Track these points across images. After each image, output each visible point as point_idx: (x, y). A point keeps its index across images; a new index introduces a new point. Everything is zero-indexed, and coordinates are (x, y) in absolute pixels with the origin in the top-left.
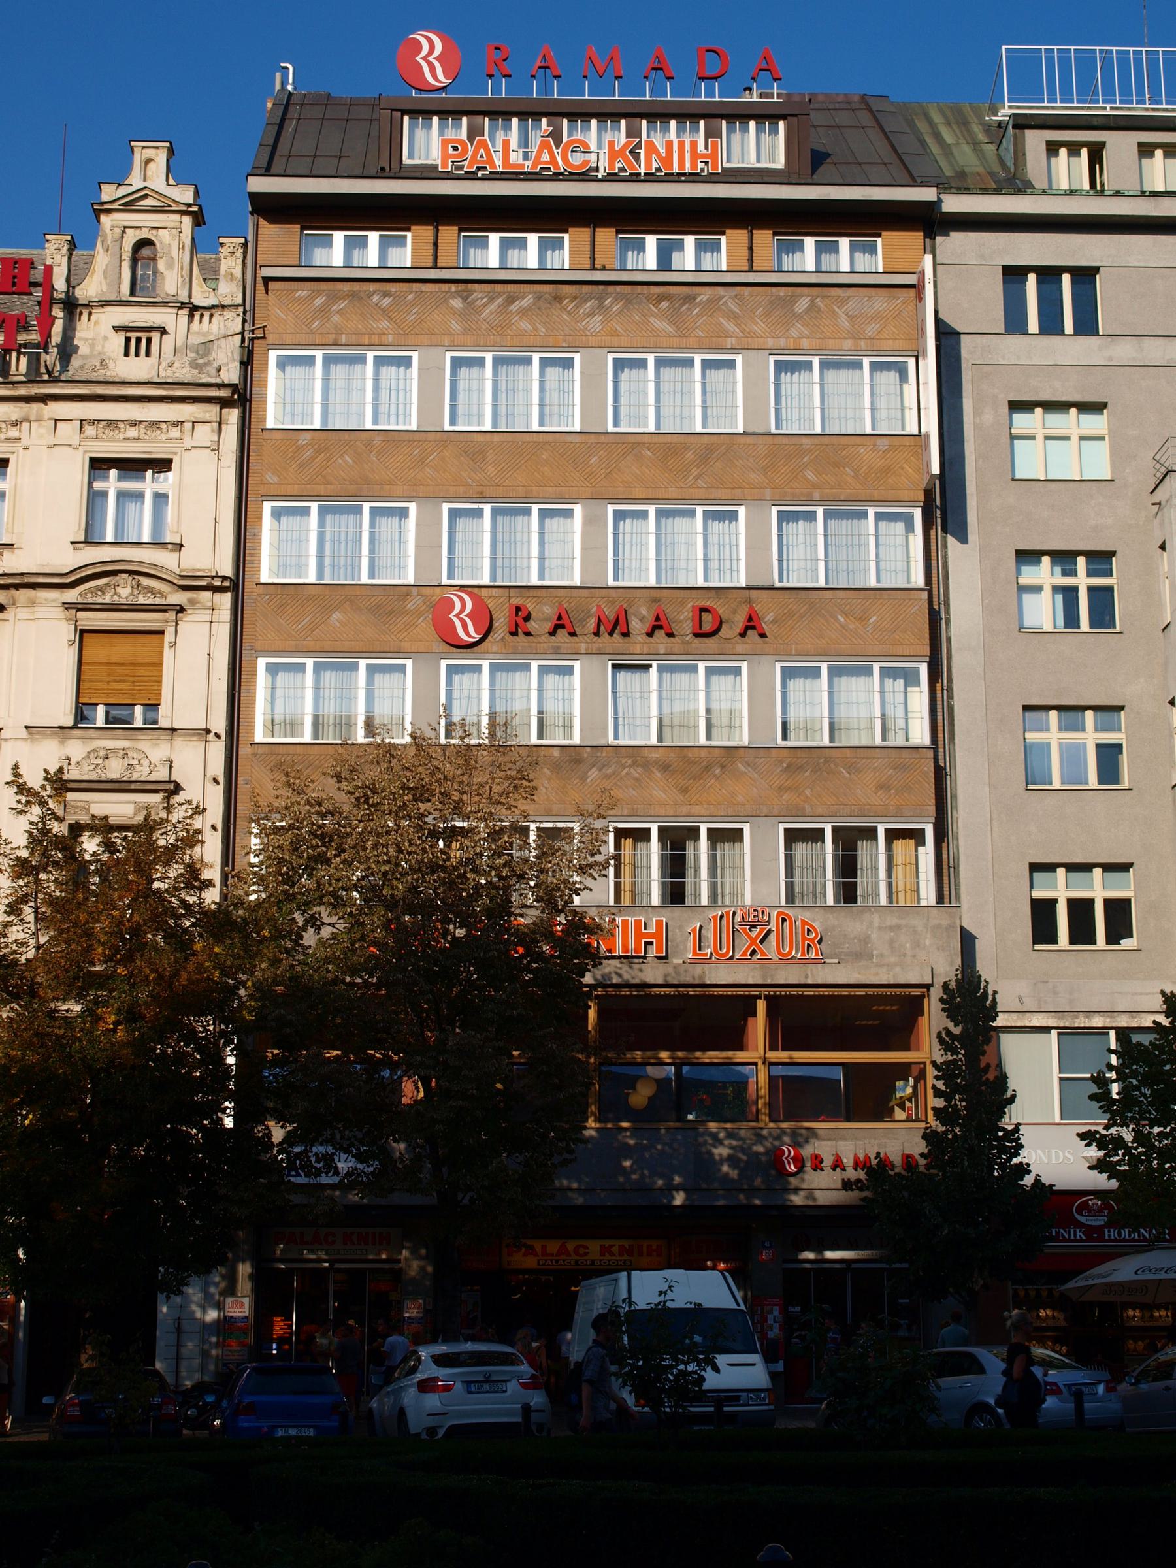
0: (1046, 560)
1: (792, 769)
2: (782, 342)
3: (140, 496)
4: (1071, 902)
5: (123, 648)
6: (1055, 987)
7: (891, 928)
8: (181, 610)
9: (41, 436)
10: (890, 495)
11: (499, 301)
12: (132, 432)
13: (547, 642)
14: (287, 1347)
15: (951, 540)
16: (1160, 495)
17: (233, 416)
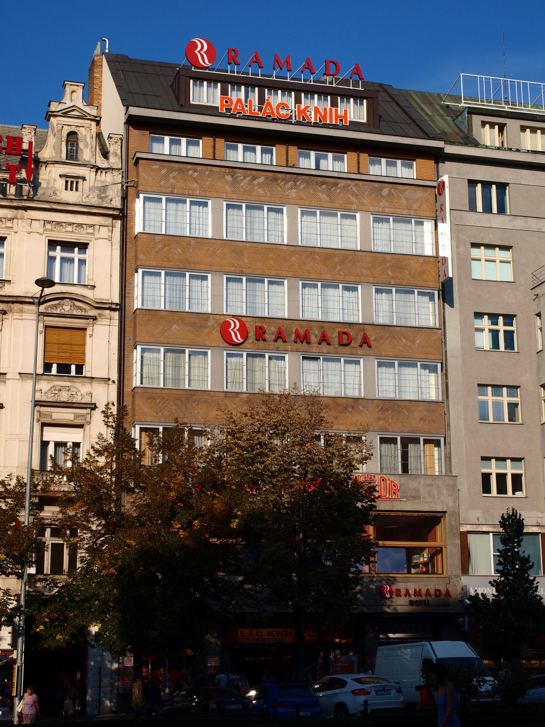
0: (486, 317)
1: (383, 410)
2: (377, 209)
3: (72, 260)
4: (513, 475)
5: (65, 336)
6: (492, 513)
7: (429, 485)
8: (95, 318)
9: (23, 227)
10: (424, 284)
11: (249, 178)
12: (69, 228)
13: (273, 345)
14: (146, 681)
15: (446, 306)
16: (537, 291)
17: (118, 223)
